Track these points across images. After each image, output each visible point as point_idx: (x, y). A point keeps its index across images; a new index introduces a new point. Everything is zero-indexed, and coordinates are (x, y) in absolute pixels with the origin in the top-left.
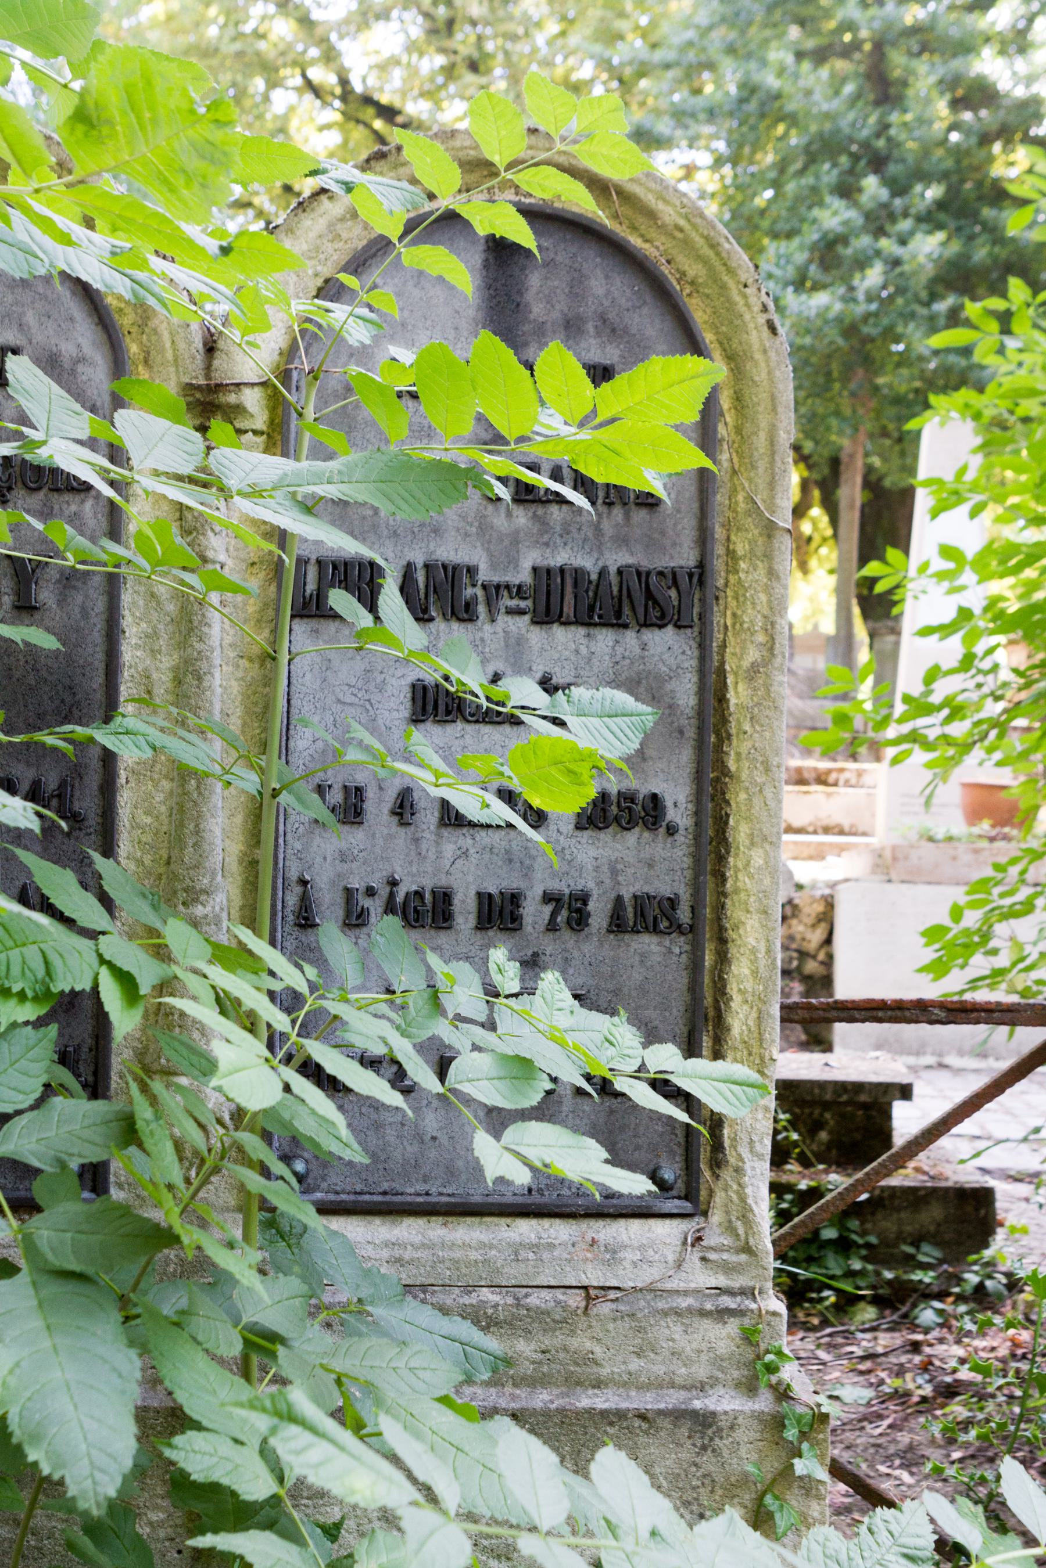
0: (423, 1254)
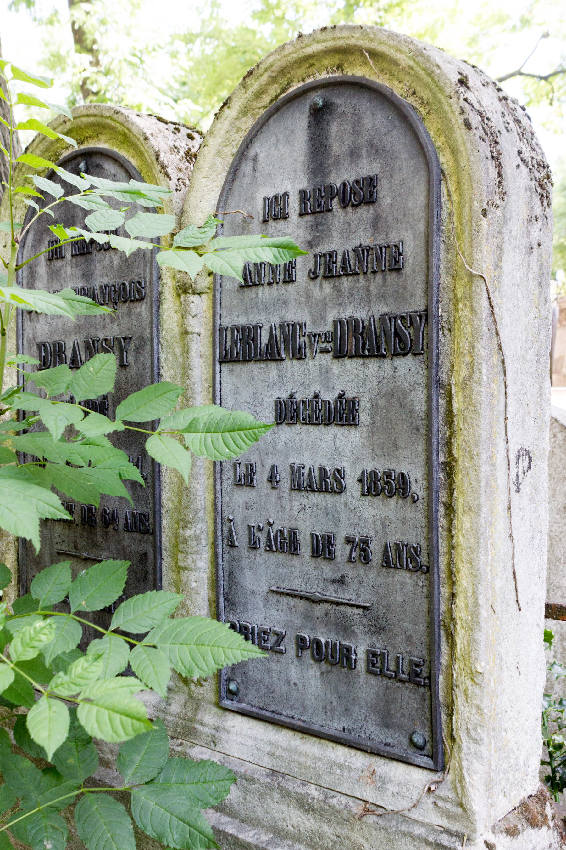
0: (284, 754)
